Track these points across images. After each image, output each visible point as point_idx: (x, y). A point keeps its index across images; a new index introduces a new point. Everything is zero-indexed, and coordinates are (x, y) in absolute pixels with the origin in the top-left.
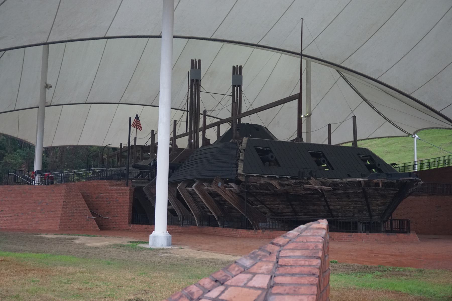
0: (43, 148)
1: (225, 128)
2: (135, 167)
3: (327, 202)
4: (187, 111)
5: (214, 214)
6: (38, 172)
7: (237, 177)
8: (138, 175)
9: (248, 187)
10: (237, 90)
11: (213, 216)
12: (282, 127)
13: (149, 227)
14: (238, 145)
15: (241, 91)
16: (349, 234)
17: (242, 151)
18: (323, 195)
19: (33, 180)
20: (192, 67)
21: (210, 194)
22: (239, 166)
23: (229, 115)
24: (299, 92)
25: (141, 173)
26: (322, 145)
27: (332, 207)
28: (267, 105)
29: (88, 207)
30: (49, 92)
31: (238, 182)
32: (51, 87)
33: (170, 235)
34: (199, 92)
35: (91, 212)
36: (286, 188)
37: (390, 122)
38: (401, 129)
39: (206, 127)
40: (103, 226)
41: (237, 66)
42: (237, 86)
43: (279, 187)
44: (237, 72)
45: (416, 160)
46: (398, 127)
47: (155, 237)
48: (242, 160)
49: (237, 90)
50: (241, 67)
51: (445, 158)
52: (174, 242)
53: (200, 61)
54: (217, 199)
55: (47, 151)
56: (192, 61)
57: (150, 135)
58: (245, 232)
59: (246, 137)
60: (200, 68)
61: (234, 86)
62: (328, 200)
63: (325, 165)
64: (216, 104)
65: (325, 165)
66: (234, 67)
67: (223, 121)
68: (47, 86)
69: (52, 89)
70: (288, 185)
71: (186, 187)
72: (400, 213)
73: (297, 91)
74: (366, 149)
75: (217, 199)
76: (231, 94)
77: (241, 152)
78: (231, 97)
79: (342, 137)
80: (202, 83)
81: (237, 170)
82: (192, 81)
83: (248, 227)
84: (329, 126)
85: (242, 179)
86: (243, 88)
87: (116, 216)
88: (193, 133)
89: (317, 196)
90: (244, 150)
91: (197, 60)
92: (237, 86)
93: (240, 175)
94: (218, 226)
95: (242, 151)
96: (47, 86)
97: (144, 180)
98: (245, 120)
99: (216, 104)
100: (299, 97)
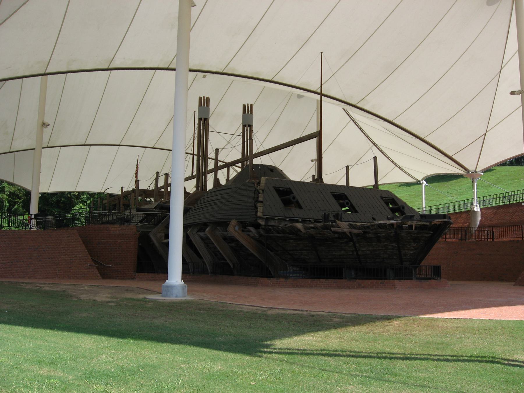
0: (40, 193)
1: (235, 171)
2: (138, 210)
3: (355, 247)
4: (193, 155)
5: (228, 261)
6: (35, 216)
7: (256, 219)
8: (143, 219)
9: (268, 231)
10: (247, 130)
11: (228, 264)
12: (297, 167)
13: (161, 276)
14: (256, 186)
15: (251, 131)
16: (380, 281)
17: (261, 192)
18: (351, 239)
19: (28, 225)
20: (200, 105)
21: (225, 239)
22: (259, 207)
23: (239, 156)
24: (319, 130)
25: (146, 217)
26: (340, 186)
27: (360, 253)
28: (283, 144)
29: (89, 253)
30: (47, 131)
31: (257, 226)
32: (49, 125)
33: (183, 283)
34: (207, 131)
35: (93, 260)
36: (312, 231)
37: (399, 168)
38: (409, 175)
39: (215, 170)
40: (106, 273)
41: (248, 104)
42: (247, 126)
43: (302, 230)
44: (248, 111)
45: (424, 206)
46: (406, 173)
47: (168, 287)
48: (262, 202)
49: (247, 130)
50: (252, 106)
51: (455, 204)
52: (190, 292)
53: (208, 99)
54: (233, 245)
55: (45, 198)
56: (200, 99)
57: (155, 176)
58: (266, 280)
59: (265, 176)
60: (208, 105)
61: (244, 126)
62: (357, 245)
63: (347, 208)
64: (225, 145)
65: (347, 208)
66: (244, 106)
67: (234, 163)
68: (44, 125)
69: (49, 129)
70: (313, 228)
71: (198, 232)
72: (431, 259)
73: (314, 129)
74: (388, 191)
75: (233, 245)
76: (241, 135)
77: (259, 193)
78: (240, 138)
79: (362, 179)
80: (210, 122)
81: (257, 212)
82: (200, 119)
83: (268, 275)
84: (347, 167)
85: (262, 222)
86: (254, 128)
87: (120, 264)
88: (201, 175)
89: (346, 240)
90: (263, 191)
91: (205, 98)
92: (247, 126)
93: (260, 218)
94: (233, 275)
95: (261, 192)
96: (44, 125)
97: (149, 224)
98: (257, 161)
99: (225, 145)
100: (318, 135)
